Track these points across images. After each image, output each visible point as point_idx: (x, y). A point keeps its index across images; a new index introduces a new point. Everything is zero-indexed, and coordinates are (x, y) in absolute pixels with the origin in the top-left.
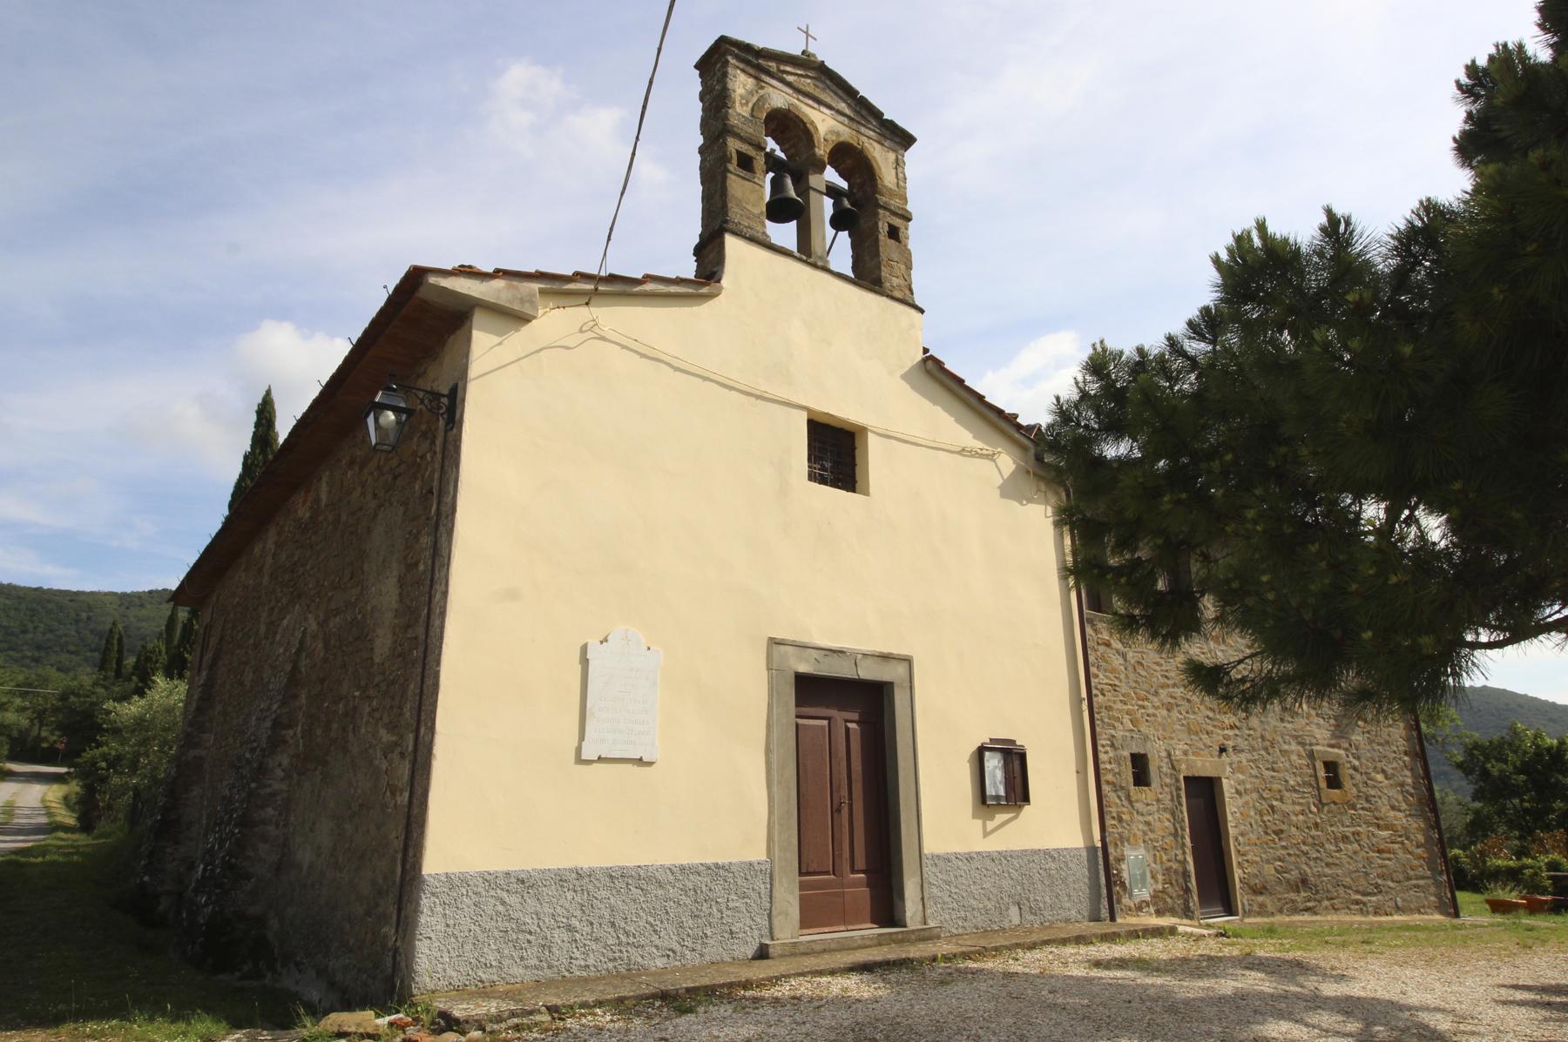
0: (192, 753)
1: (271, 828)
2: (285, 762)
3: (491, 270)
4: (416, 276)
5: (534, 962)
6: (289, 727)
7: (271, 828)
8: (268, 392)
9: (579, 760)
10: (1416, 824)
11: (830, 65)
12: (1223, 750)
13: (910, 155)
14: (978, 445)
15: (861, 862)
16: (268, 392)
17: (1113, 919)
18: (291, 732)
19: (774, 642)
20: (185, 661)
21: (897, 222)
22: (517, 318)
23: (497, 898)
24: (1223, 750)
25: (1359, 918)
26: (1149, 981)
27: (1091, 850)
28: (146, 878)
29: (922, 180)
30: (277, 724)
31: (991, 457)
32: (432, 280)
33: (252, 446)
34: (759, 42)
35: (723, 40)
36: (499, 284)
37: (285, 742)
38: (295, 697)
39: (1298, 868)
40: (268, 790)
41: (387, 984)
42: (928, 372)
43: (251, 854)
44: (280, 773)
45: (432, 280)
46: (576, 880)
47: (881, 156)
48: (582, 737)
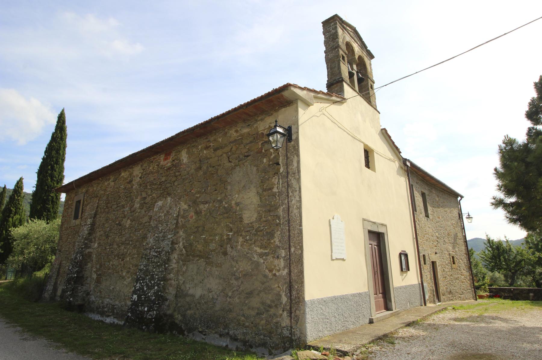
0: (88, 250)
1: (173, 281)
2: (176, 257)
3: (303, 87)
4: (287, 87)
5: (329, 329)
6: (177, 244)
7: (173, 281)
8: (63, 110)
9: (332, 260)
10: (468, 274)
11: (357, 29)
12: (436, 253)
13: (372, 61)
14: (392, 157)
15: (381, 292)
16: (63, 110)
17: (425, 305)
18: (177, 246)
19: (364, 220)
20: (11, 210)
21: (372, 83)
22: (308, 104)
23: (321, 308)
24: (436, 253)
25: (460, 302)
26: (476, 325)
27: (419, 284)
28: (71, 299)
29: (378, 70)
30: (173, 243)
31: (394, 162)
32: (292, 89)
33: (56, 130)
34: (344, 19)
35: (336, 15)
36: (305, 92)
37: (176, 249)
38: (178, 232)
39: (53, 274)
40: (171, 267)
41: (296, 342)
42: (383, 133)
43: (167, 291)
44: (175, 261)
45: (292, 89)
46: (334, 300)
47: (366, 59)
48: (332, 252)
